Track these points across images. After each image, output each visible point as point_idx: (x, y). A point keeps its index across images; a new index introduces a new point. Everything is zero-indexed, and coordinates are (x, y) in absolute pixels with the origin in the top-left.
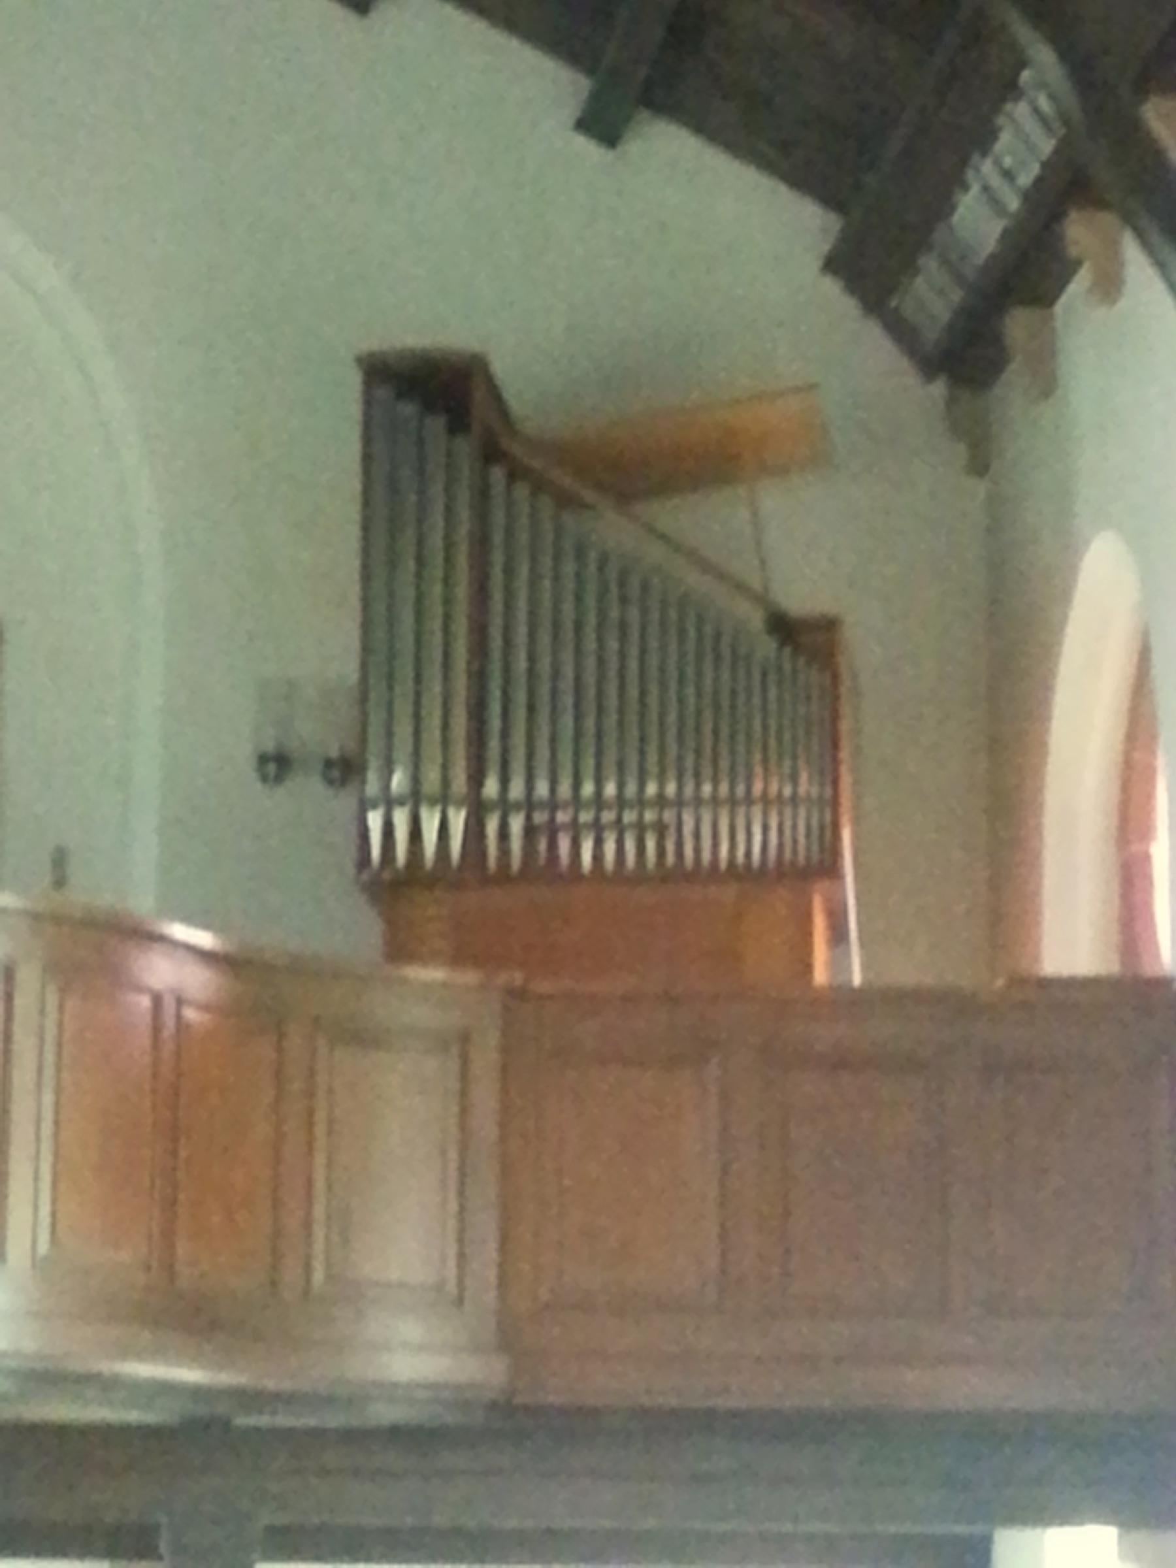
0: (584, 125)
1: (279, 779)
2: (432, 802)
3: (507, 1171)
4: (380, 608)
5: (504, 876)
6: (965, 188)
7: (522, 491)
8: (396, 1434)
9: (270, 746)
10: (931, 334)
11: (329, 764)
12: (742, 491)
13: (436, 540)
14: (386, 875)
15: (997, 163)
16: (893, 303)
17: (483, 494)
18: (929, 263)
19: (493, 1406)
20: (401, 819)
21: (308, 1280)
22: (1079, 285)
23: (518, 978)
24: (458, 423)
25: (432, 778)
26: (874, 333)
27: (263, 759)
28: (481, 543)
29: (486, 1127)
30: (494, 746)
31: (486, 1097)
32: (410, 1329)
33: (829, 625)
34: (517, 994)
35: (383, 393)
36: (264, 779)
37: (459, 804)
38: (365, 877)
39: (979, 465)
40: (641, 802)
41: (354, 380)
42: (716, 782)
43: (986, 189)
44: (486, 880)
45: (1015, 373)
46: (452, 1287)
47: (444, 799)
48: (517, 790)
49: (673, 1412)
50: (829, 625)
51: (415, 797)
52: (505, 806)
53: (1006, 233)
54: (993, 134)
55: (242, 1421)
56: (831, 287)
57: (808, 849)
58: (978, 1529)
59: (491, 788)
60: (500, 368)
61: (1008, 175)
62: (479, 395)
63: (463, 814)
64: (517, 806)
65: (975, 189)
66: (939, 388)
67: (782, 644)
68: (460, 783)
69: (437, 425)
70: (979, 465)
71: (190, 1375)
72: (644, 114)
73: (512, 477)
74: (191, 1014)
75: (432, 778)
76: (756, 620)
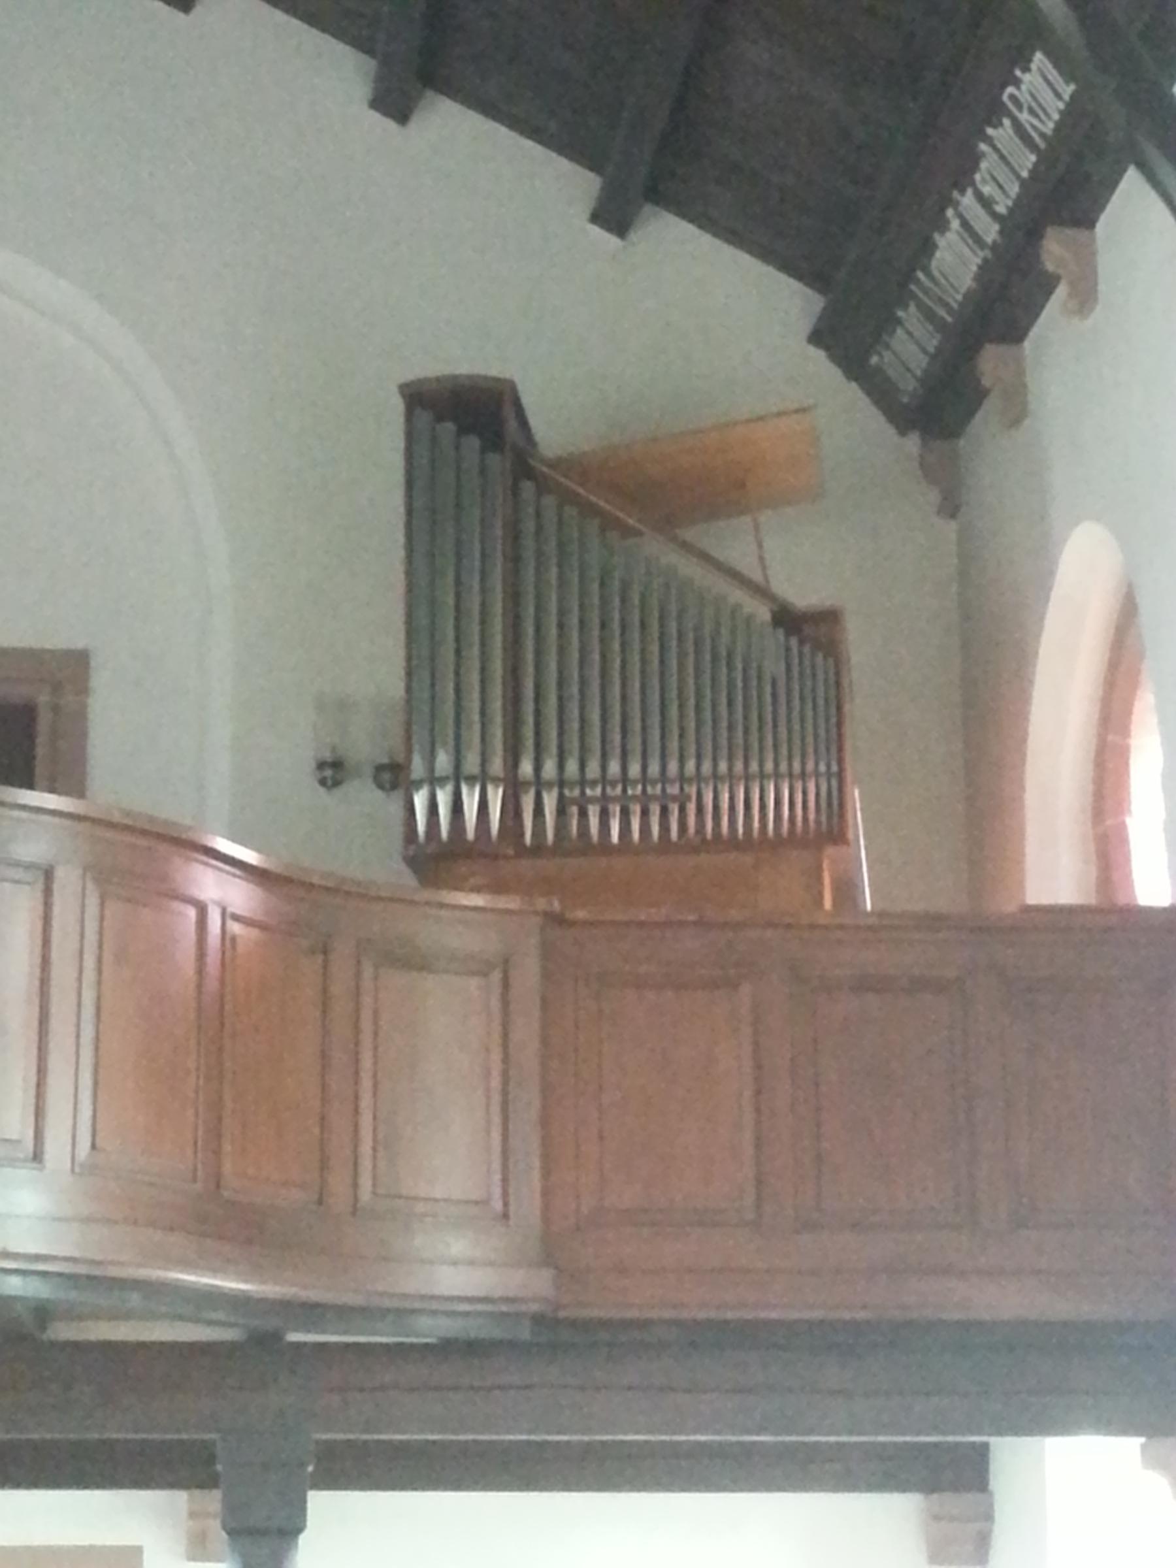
0: (596, 218)
1: (337, 783)
2: (471, 780)
3: (547, 1089)
4: (423, 620)
5: (538, 849)
6: (943, 227)
7: (549, 501)
8: (446, 1349)
9: (328, 756)
10: (908, 385)
11: (379, 769)
12: (747, 519)
13: (474, 604)
14: (430, 849)
15: (980, 197)
16: (874, 360)
17: (515, 491)
18: (910, 315)
19: (538, 1320)
20: (443, 799)
21: (356, 1199)
22: (1061, 291)
23: (556, 905)
24: (494, 439)
25: (472, 763)
26: (853, 392)
27: (321, 765)
28: (514, 535)
29: (528, 1055)
30: (528, 732)
31: (526, 1029)
32: (458, 1245)
33: (830, 617)
34: (557, 920)
35: (424, 418)
36: (323, 782)
37: (496, 781)
38: (412, 850)
39: (951, 507)
40: (583, 782)
41: (397, 405)
42: (731, 759)
43: (965, 224)
44: (522, 851)
45: (986, 420)
46: (498, 1205)
47: (483, 779)
48: (550, 769)
49: (709, 1324)
50: (830, 617)
51: (458, 777)
52: (539, 784)
53: (984, 267)
54: (975, 160)
55: (63, 1332)
56: (818, 355)
57: (818, 822)
58: (984, 1439)
59: (526, 768)
60: (528, 401)
61: (986, 203)
62: (508, 412)
63: (500, 791)
64: (549, 785)
65: (955, 224)
66: (912, 443)
67: (788, 634)
68: (497, 766)
69: (473, 443)
70: (951, 507)
71: (242, 1286)
72: (648, 208)
73: (541, 490)
74: (235, 928)
75: (472, 763)
76: (764, 613)
